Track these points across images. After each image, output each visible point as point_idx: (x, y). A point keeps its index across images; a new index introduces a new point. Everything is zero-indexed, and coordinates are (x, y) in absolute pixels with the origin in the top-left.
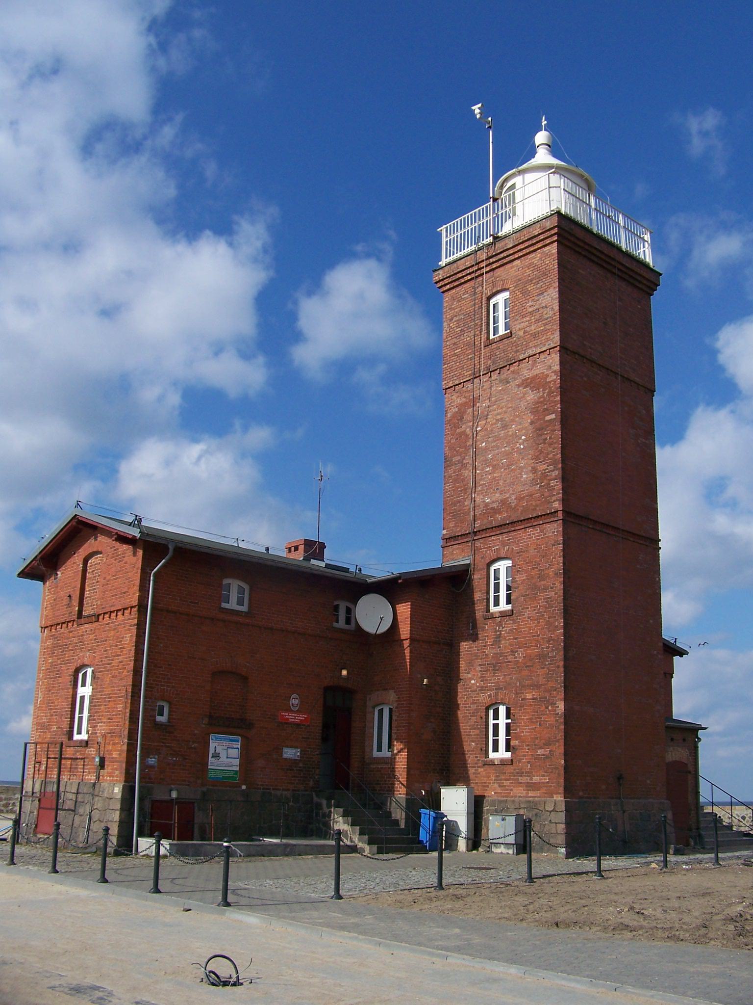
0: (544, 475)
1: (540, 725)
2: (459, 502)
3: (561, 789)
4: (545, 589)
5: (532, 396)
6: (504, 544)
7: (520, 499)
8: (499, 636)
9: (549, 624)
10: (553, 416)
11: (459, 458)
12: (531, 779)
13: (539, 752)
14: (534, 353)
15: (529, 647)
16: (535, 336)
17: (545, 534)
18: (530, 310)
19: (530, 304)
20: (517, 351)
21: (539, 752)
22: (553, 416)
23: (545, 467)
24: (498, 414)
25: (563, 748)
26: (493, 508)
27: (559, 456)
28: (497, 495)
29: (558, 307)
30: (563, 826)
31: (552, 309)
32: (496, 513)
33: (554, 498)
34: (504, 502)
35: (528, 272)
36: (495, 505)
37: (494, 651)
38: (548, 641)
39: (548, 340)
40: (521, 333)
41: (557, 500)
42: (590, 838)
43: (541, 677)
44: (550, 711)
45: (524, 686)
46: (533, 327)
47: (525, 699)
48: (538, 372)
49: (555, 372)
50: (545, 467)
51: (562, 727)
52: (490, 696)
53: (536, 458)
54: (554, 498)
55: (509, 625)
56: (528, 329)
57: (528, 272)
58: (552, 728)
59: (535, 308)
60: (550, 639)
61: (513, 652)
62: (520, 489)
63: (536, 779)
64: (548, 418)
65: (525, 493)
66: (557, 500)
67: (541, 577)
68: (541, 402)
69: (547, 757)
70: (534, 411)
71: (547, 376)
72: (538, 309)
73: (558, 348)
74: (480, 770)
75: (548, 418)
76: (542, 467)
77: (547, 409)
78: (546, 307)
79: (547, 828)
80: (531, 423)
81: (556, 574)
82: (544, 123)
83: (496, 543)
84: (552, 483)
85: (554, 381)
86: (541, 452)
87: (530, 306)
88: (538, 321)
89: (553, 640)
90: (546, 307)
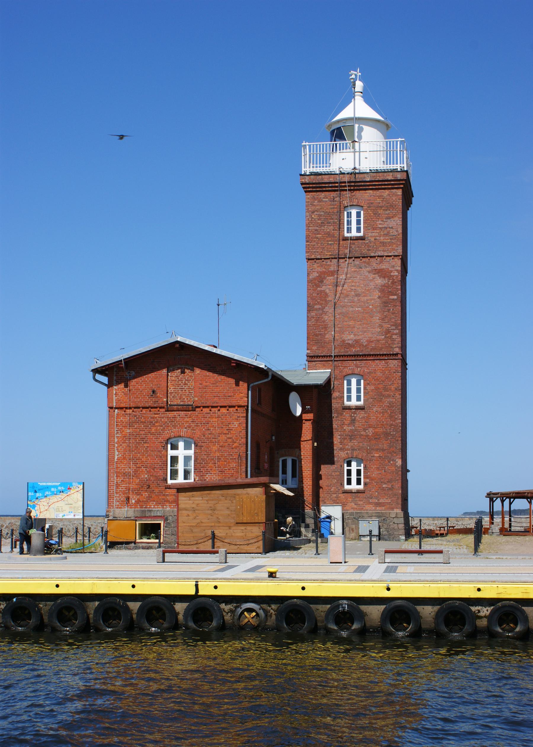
0: (388, 331)
1: (385, 471)
2: (321, 334)
3: (400, 506)
4: (389, 396)
5: (380, 281)
6: (357, 367)
7: (369, 342)
8: (354, 420)
9: (391, 417)
10: (395, 297)
11: (320, 307)
12: (379, 500)
13: (384, 486)
14: (382, 254)
15: (376, 428)
16: (383, 244)
17: (388, 365)
18: (380, 226)
19: (380, 222)
20: (369, 250)
21: (384, 486)
22: (395, 297)
23: (389, 326)
24: (353, 286)
25: (400, 484)
26: (349, 344)
27: (400, 322)
28: (352, 336)
29: (401, 231)
30: (403, 525)
31: (397, 231)
32: (351, 347)
33: (395, 346)
34: (357, 341)
35: (379, 200)
36: (350, 342)
37: (350, 428)
38: (390, 426)
39: (393, 249)
40: (373, 239)
41: (397, 347)
42: (20, 554)
43: (385, 445)
44: (391, 464)
45: (373, 449)
46: (382, 238)
47: (374, 456)
48: (384, 267)
49: (397, 270)
50: (389, 326)
51: (400, 473)
52: (347, 453)
53: (383, 319)
54: (395, 346)
55: (361, 415)
56: (378, 238)
57: (379, 200)
58: (393, 473)
59: (383, 226)
60: (392, 425)
61: (365, 430)
62: (370, 335)
63: (381, 501)
64: (392, 297)
65: (374, 339)
66: (397, 347)
67: (386, 389)
68: (386, 286)
69: (390, 489)
70: (382, 291)
71: (391, 271)
72: (386, 228)
73: (400, 257)
74: (340, 495)
75: (392, 297)
76: (386, 326)
77: (390, 292)
78: (392, 228)
79: (392, 526)
80: (379, 297)
81: (396, 389)
82: (359, 85)
83: (351, 366)
84: (394, 337)
85: (397, 276)
86: (386, 316)
87: (379, 223)
88: (385, 235)
89: (394, 425)
90: (392, 228)
